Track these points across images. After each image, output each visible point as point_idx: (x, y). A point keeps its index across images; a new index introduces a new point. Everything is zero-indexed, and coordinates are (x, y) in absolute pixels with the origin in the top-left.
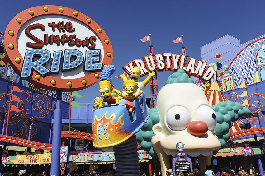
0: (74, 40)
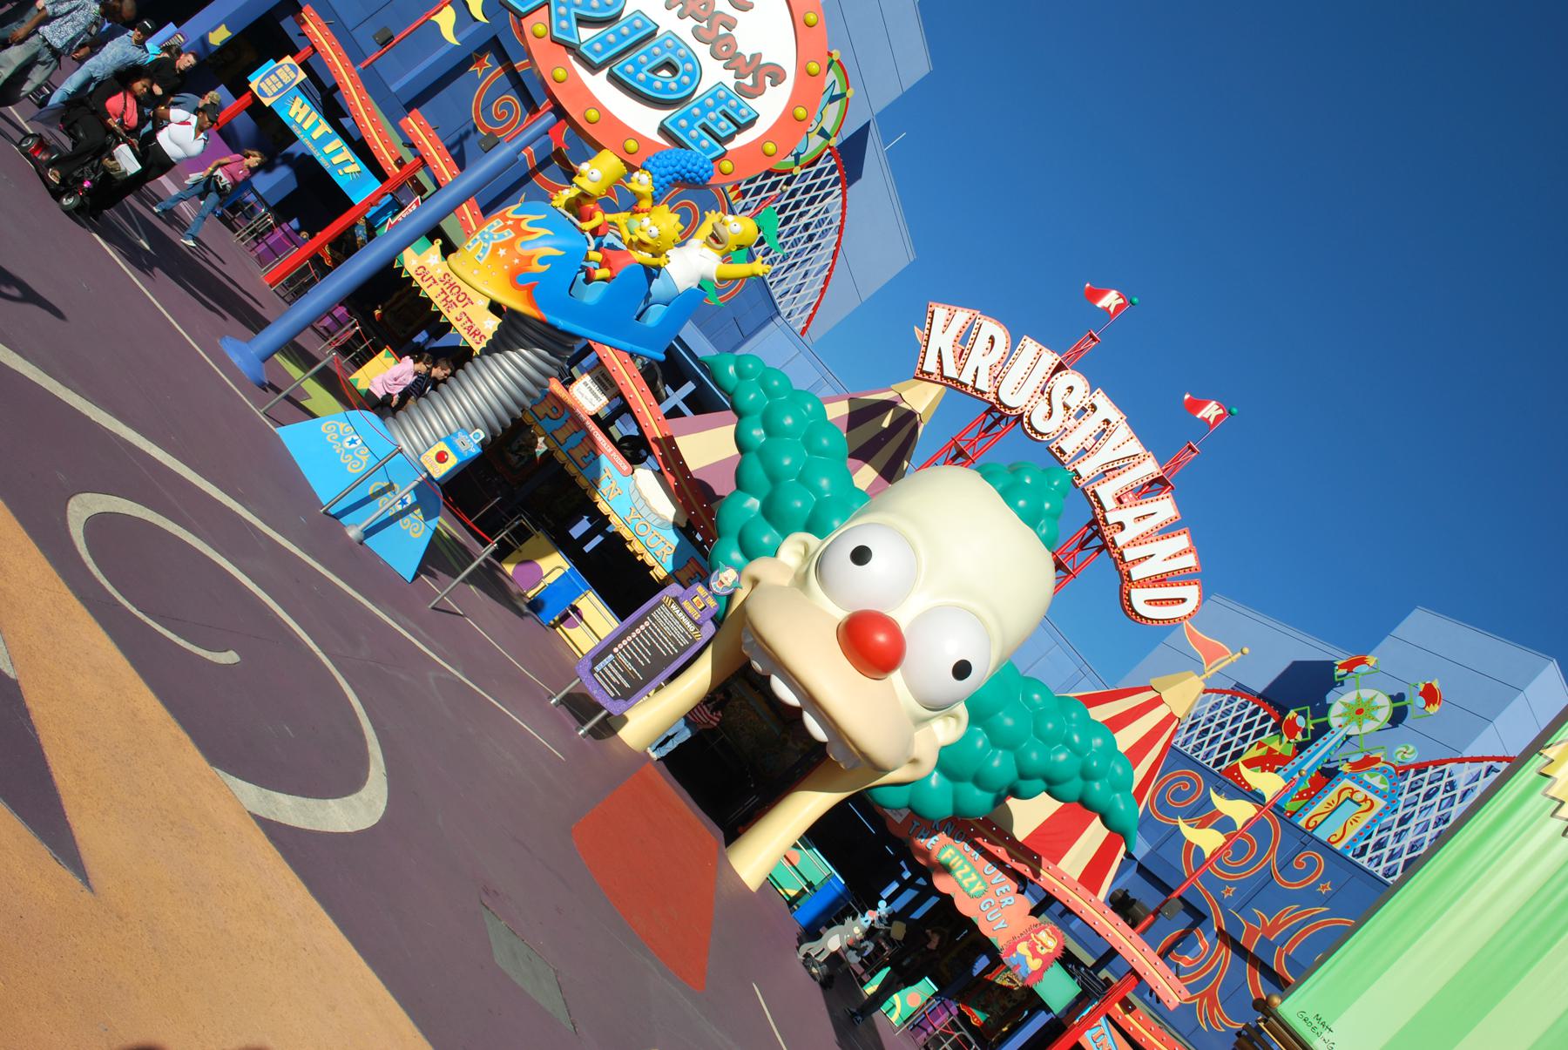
0: (722, 30)
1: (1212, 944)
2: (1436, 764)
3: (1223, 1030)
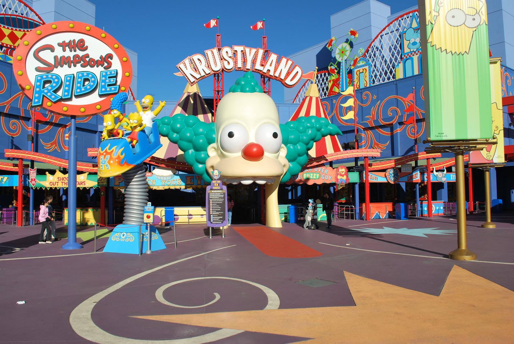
0: (87, 59)
1: (365, 133)
2: (369, 47)
3: (385, 148)
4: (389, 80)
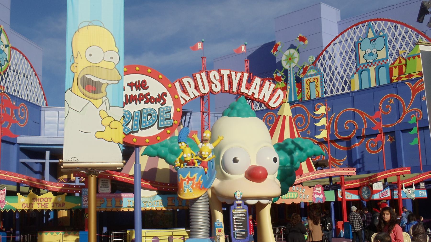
0: (149, 97)
3: (343, 163)
4: (344, 91)
